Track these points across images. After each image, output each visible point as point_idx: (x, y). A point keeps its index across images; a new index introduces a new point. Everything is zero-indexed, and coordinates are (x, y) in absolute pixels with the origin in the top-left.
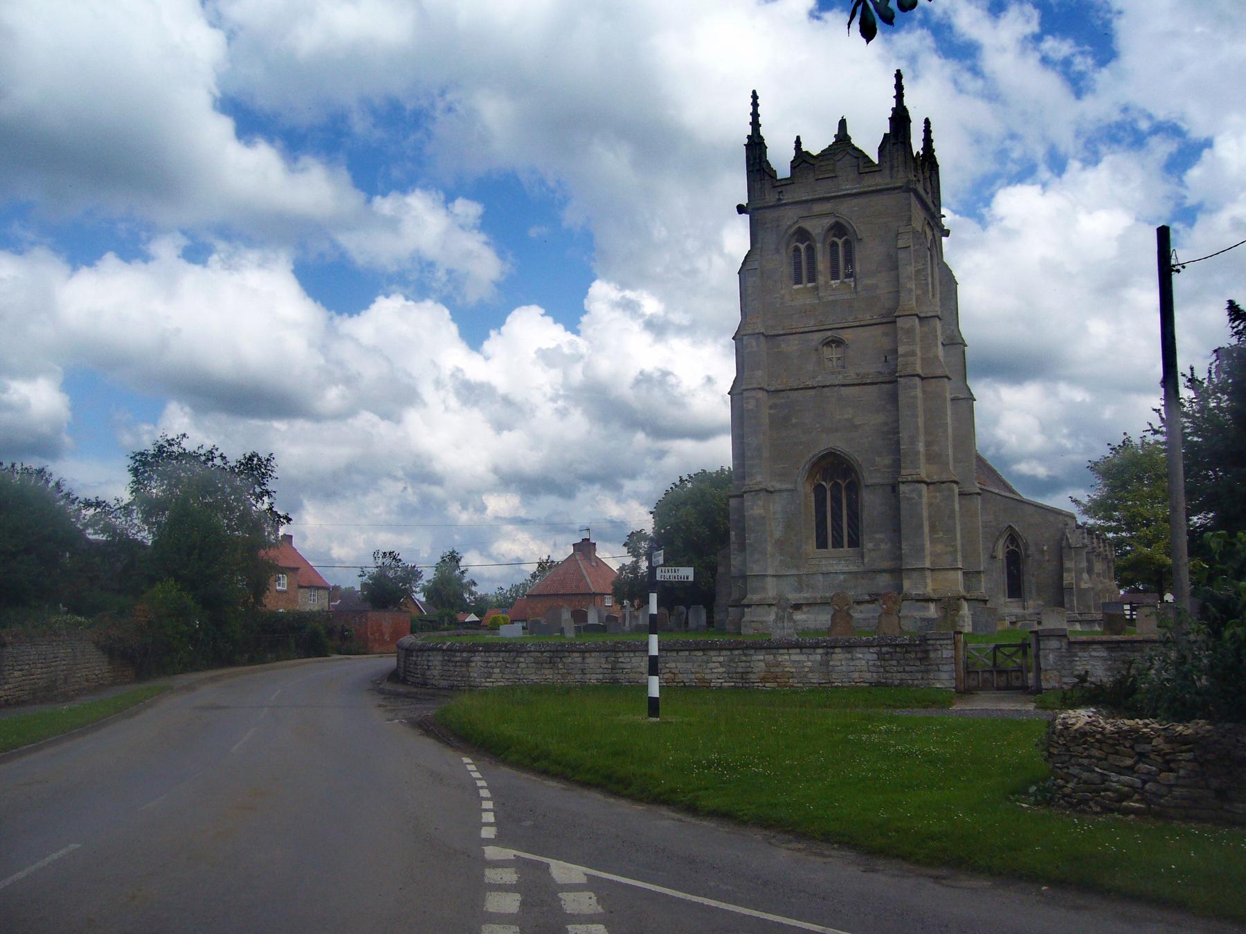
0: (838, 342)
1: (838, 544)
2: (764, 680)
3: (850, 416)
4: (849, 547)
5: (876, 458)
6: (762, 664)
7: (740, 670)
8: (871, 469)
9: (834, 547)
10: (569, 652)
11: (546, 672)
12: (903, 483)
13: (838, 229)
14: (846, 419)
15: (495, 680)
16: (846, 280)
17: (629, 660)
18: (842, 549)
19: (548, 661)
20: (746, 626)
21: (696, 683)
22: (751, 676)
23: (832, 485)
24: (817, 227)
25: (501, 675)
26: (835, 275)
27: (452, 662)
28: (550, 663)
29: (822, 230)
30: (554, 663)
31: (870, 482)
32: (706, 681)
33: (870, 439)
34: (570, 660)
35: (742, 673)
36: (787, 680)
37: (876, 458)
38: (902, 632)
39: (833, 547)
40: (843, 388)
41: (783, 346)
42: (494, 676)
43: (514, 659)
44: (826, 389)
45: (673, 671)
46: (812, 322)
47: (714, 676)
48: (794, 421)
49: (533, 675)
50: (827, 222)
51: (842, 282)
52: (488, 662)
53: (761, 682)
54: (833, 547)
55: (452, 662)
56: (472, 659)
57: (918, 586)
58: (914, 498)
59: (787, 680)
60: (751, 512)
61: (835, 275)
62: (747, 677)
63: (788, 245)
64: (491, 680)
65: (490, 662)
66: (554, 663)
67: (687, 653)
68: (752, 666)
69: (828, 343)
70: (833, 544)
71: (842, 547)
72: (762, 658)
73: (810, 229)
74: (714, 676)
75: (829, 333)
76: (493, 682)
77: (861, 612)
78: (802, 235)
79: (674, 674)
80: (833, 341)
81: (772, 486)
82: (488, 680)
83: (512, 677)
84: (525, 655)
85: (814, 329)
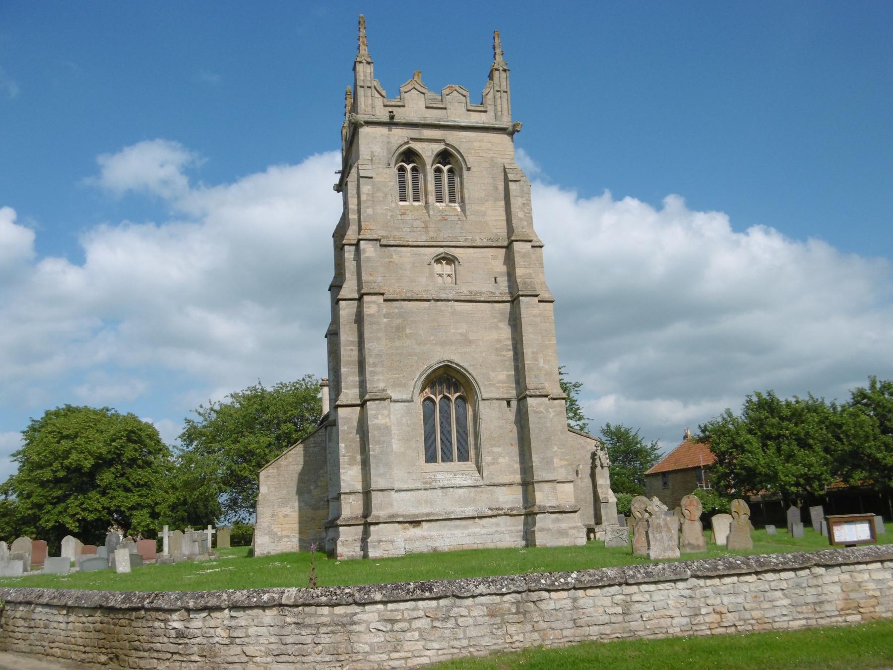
0: (450, 260)
1: (447, 458)
2: (842, 612)
3: (465, 331)
4: (459, 461)
5: (491, 373)
6: (837, 589)
7: (810, 599)
8: (486, 383)
9: (443, 461)
10: (549, 591)
11: (512, 629)
12: (531, 396)
13: (445, 156)
14: (460, 334)
15: (410, 655)
16: (451, 204)
17: (647, 596)
18: (452, 463)
19: (514, 611)
20: (374, 547)
21: (752, 625)
22: (827, 607)
23: (441, 398)
24: (428, 152)
25: (423, 643)
26: (439, 199)
27: (310, 626)
28: (517, 613)
29: (432, 154)
30: (525, 613)
31: (485, 396)
32: (767, 620)
33: (484, 354)
34: (552, 605)
35: (815, 604)
36: (872, 609)
37: (491, 373)
38: (184, 555)
39: (442, 461)
40: (456, 303)
41: (394, 257)
42: (407, 646)
43: (448, 611)
44: (439, 303)
45: (718, 609)
46: (424, 238)
47: (778, 612)
48: (408, 331)
49: (487, 639)
50: (440, 147)
51: (447, 205)
52: (393, 621)
53: (841, 616)
54: (442, 461)
55: (310, 626)
56: (355, 618)
57: (549, 498)
58: (542, 412)
59: (872, 609)
60: (376, 421)
61: (439, 199)
62: (822, 609)
63: (396, 163)
64: (402, 654)
65: (397, 621)
66: (525, 613)
67: (735, 579)
68: (825, 591)
69: (438, 260)
70: (442, 458)
71: (452, 461)
72: (836, 579)
73: (420, 151)
74: (778, 612)
75: (441, 250)
76: (406, 658)
77: (484, 527)
78: (409, 155)
79: (721, 613)
80: (444, 259)
81: (147, 435)
82: (395, 655)
83: (445, 645)
84: (469, 602)
85: (426, 244)
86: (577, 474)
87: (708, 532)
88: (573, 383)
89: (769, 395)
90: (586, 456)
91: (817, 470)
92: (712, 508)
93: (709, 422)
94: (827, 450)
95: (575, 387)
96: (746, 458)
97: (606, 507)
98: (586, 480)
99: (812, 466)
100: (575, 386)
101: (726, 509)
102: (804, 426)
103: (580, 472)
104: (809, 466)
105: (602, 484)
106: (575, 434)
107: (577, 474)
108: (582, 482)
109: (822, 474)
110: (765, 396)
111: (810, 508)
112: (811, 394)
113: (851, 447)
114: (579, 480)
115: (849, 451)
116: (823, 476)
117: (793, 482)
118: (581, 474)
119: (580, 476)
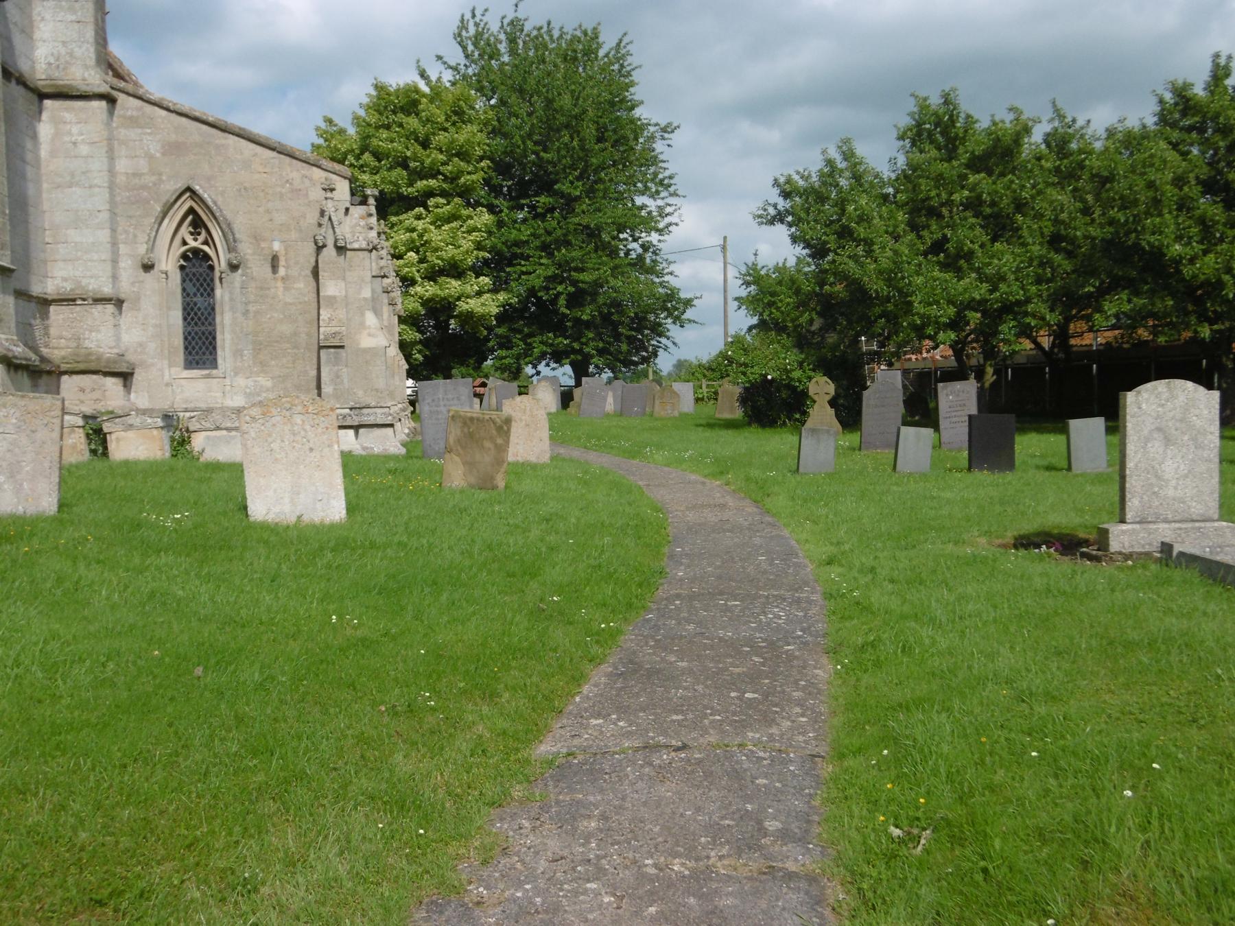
86: (274, 268)
87: (1115, 439)
88: (662, 126)
89: (947, 102)
90: (304, 216)
91: (1012, 290)
92: (761, 375)
93: (798, 173)
94: (1055, 241)
95: (665, 132)
96: (849, 257)
97: (337, 361)
98: (301, 285)
99: (1003, 278)
100: (664, 130)
101: (792, 379)
102: (1012, 182)
103: (282, 262)
104: (995, 281)
105: (334, 297)
106: (274, 154)
107: (274, 268)
108: (286, 289)
109: (1028, 301)
110: (935, 101)
111: (940, 385)
112: (1059, 105)
113: (1111, 230)
114: (280, 284)
115: (1103, 240)
116: (1030, 308)
117: (944, 320)
118: (287, 267)
119: (282, 271)
